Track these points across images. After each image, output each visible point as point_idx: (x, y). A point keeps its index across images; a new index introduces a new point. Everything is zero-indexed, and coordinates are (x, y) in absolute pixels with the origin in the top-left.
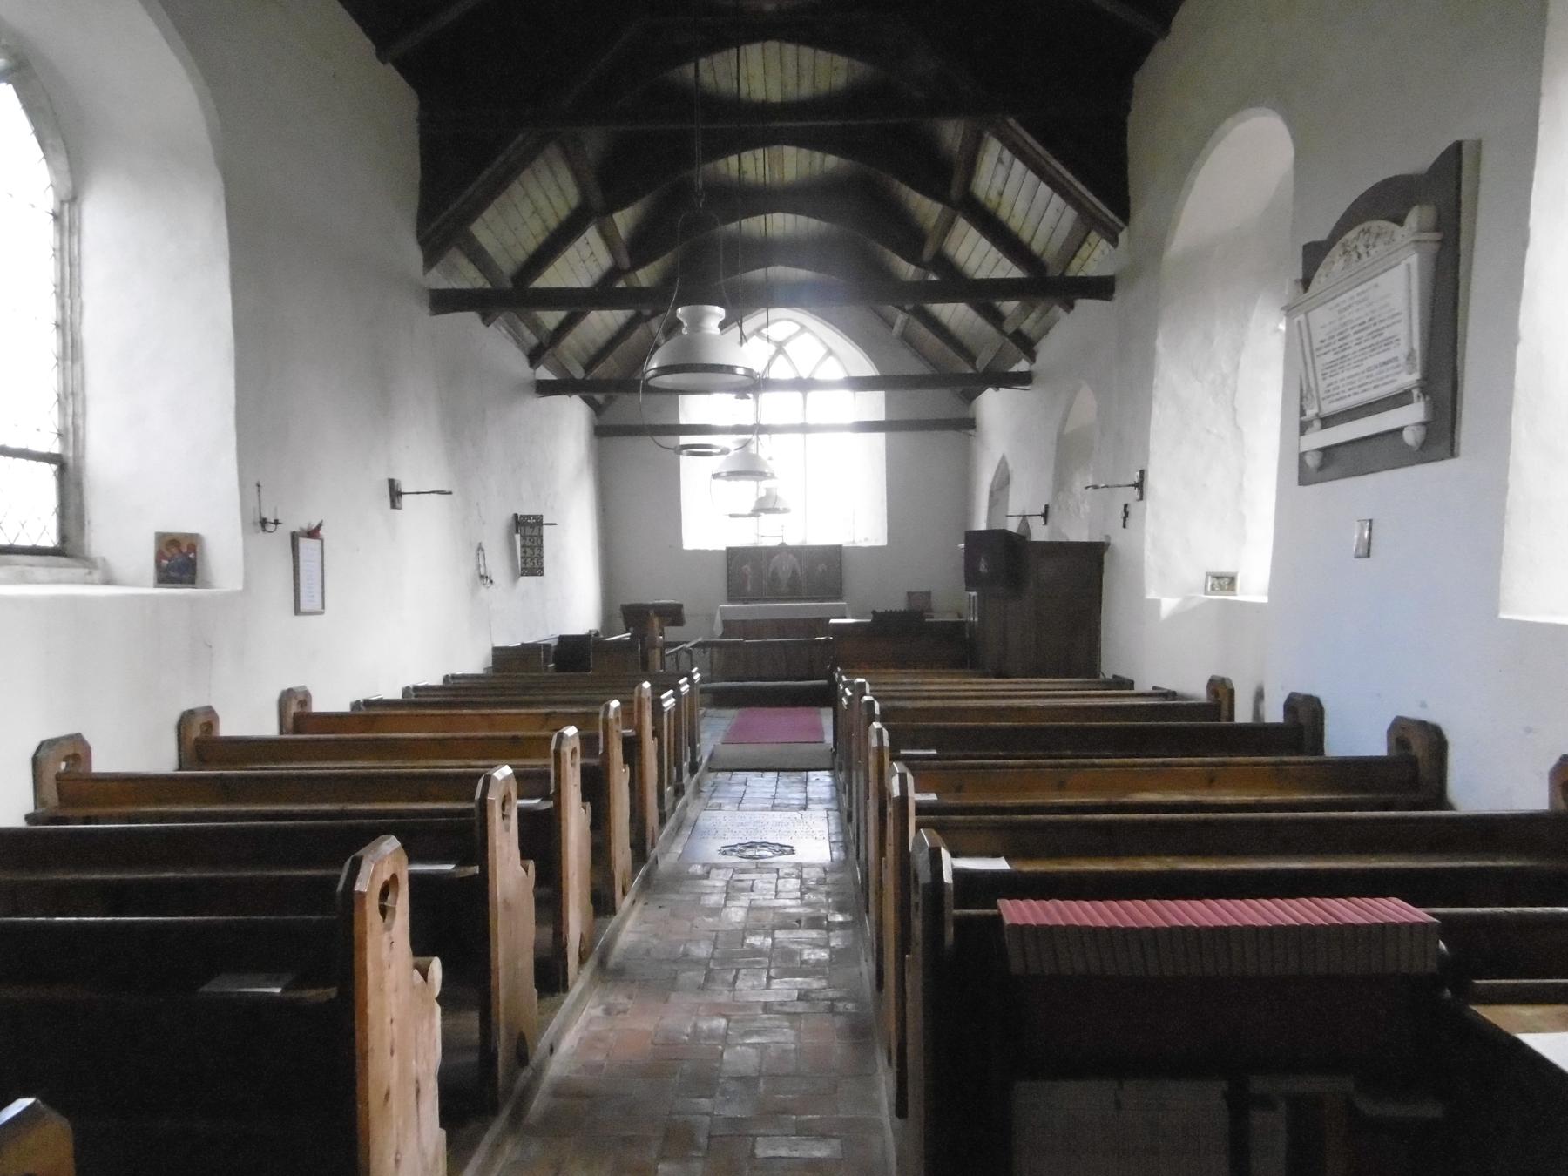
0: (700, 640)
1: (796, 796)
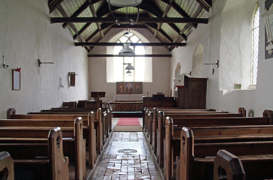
0: (111, 102)
1: (135, 138)
